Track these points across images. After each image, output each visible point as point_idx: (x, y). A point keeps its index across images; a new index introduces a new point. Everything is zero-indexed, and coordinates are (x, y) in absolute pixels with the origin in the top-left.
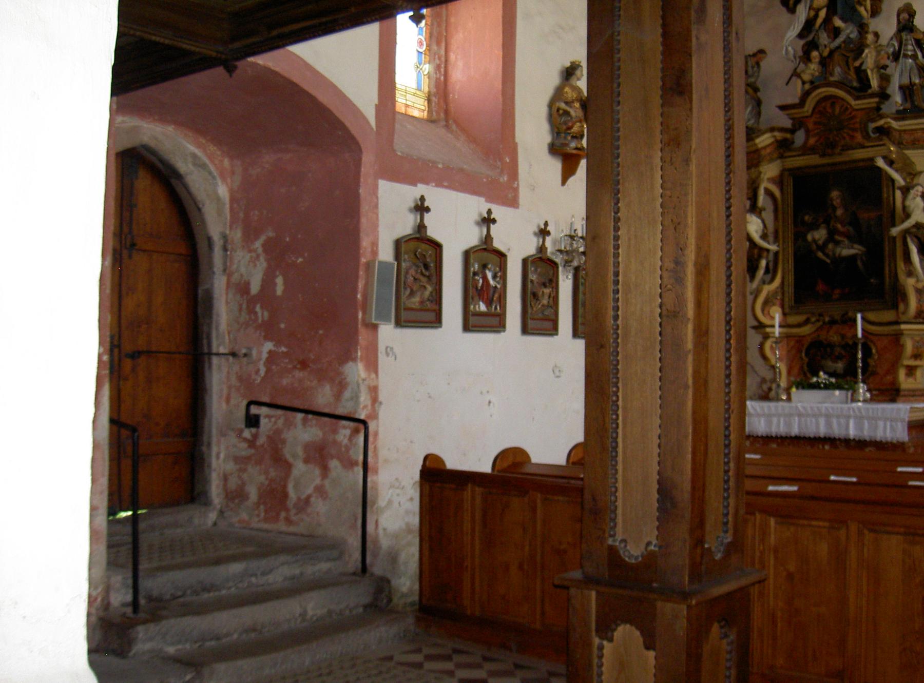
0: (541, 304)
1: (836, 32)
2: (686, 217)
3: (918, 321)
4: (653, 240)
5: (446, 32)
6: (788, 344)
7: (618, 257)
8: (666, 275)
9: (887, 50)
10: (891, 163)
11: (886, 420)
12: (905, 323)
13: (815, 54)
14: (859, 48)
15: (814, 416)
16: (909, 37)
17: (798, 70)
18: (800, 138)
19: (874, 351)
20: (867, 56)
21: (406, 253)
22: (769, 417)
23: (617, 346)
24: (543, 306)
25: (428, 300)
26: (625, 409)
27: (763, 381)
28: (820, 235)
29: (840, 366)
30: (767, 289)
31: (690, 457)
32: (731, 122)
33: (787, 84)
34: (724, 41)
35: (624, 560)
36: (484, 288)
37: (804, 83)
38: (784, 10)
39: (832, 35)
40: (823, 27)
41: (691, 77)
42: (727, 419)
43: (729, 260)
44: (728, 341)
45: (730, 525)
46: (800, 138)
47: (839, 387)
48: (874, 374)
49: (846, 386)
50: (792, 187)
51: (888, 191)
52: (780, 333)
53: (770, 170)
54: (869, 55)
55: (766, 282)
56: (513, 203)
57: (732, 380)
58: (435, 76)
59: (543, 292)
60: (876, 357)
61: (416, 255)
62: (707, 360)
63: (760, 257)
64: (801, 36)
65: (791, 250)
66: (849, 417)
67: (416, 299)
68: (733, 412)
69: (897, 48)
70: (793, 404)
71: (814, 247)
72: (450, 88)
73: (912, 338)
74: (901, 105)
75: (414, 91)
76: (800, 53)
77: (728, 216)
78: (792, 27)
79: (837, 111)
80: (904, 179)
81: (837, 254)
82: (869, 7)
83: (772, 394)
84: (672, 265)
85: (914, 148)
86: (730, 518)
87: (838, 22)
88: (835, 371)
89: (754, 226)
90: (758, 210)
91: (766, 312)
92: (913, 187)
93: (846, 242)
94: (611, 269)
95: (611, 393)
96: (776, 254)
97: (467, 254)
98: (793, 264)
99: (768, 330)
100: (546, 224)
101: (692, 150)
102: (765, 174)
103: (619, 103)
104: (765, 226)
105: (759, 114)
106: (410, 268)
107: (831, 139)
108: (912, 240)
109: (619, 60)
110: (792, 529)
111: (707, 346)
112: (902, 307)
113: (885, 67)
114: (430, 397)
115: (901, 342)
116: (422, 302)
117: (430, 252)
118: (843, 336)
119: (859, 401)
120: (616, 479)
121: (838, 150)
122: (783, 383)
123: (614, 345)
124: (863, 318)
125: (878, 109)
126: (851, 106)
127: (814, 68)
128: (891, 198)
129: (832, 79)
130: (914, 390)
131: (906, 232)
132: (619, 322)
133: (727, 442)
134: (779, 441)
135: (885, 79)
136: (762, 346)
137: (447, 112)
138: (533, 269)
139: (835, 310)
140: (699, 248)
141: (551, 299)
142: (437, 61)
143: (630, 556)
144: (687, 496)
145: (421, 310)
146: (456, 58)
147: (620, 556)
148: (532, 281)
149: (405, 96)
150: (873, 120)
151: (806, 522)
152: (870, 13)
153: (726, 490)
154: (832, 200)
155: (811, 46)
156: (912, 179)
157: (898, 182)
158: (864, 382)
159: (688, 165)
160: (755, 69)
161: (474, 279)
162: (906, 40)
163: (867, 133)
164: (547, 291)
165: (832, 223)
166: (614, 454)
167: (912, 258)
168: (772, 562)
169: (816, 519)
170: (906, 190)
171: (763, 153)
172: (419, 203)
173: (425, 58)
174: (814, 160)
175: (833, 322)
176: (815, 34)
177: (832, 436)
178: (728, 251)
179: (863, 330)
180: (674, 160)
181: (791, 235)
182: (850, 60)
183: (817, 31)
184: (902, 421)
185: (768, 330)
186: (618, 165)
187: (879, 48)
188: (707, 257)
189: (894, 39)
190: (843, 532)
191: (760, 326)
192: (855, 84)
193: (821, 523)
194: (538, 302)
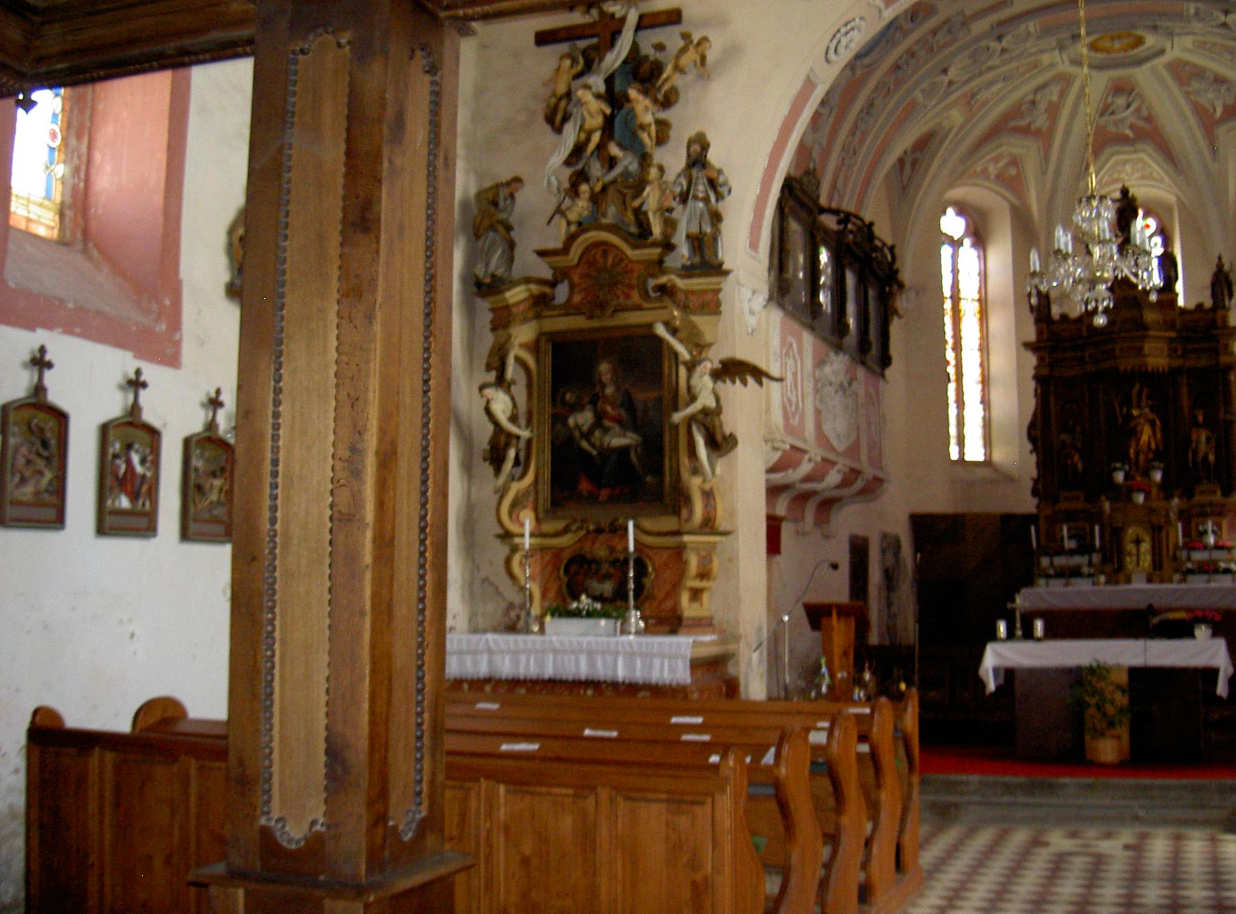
0: (209, 500)
1: (612, 162)
2: (367, 390)
3: (704, 530)
4: (323, 419)
5: (91, 122)
6: (542, 558)
7: (278, 439)
8: (339, 465)
9: (673, 189)
10: (674, 331)
11: (663, 656)
12: (690, 533)
13: (584, 188)
14: (640, 185)
15: (573, 652)
16: (700, 175)
17: (563, 207)
18: (562, 293)
19: (650, 569)
20: (648, 195)
21: (16, 424)
22: (515, 653)
23: (274, 559)
24: (212, 503)
25: (47, 491)
26: (283, 642)
27: (511, 606)
28: (584, 418)
29: (607, 588)
30: (516, 488)
31: (367, 707)
32: (432, 271)
33: (549, 223)
34: (429, 166)
35: (280, 846)
36: (129, 477)
37: (569, 223)
38: (548, 128)
39: (607, 166)
40: (596, 153)
41: (380, 209)
42: (421, 656)
43: (425, 448)
44: (422, 554)
45: (424, 795)
46: (562, 293)
47: (604, 614)
48: (651, 597)
49: (614, 614)
50: (550, 356)
51: (670, 368)
52: (531, 545)
53: (523, 333)
54: (651, 195)
55: (516, 478)
56: (173, 360)
57: (427, 604)
58: (71, 181)
59: (212, 485)
60: (653, 576)
61: (29, 427)
62: (392, 577)
63: (507, 445)
64: (568, 162)
65: (547, 438)
66: (617, 653)
67: (28, 491)
68: (427, 645)
69: (685, 188)
70: (546, 638)
71: (577, 434)
72: (92, 199)
73: (698, 554)
74: (689, 258)
75: (40, 200)
76: (566, 185)
77: (425, 392)
78: (557, 151)
79: (610, 260)
80: (690, 353)
81: (606, 444)
82: (653, 134)
83: (521, 624)
84: (348, 453)
85: (703, 314)
86: (425, 786)
87: (614, 150)
88: (601, 595)
89: (501, 404)
90: (506, 384)
91: (514, 516)
92: (700, 362)
93: (617, 428)
94: (269, 456)
95: (265, 622)
96: (529, 442)
97: (105, 429)
98: (550, 456)
99: (517, 540)
100: (218, 392)
101: (377, 306)
102: (515, 338)
103: (286, 237)
104: (515, 405)
105: (511, 260)
106: (22, 445)
107: (601, 297)
108: (699, 430)
109: (289, 182)
110: (527, 799)
111: (392, 561)
112: (684, 513)
113: (670, 210)
114: (46, 627)
115: (685, 557)
116: (37, 493)
117: (51, 423)
118: (612, 550)
119: (629, 633)
120: (271, 737)
121: (609, 312)
122: (536, 610)
123: (270, 557)
124: (635, 526)
125: (661, 262)
126: (626, 256)
127: (582, 206)
128: (674, 376)
129: (605, 221)
130: (701, 619)
131: (691, 419)
132: (278, 527)
133: (420, 686)
134: (530, 685)
135: (670, 225)
136: (508, 562)
137: (86, 233)
138: (198, 452)
139: (600, 515)
140: (383, 431)
141: (223, 494)
142: (76, 162)
143: (290, 841)
144: (363, 757)
145: (35, 505)
146: (103, 158)
147: (276, 842)
148: (196, 470)
149: (27, 206)
150: (654, 276)
151: (544, 790)
152: (654, 141)
153: (419, 749)
154: (600, 375)
155: (581, 177)
156: (700, 353)
157: (683, 356)
158: (637, 608)
159: (371, 323)
160: (508, 202)
161: (113, 463)
162: (697, 178)
163: (646, 292)
164: (217, 483)
165: (600, 404)
166: (268, 703)
167: (697, 452)
168: (502, 844)
169: (557, 785)
170: (691, 367)
171: (514, 310)
172: (38, 355)
173: (59, 155)
174: (577, 322)
175: (599, 531)
176: (586, 163)
177: (596, 678)
178: (425, 437)
179: (636, 540)
180: (353, 315)
181: (547, 418)
182: (628, 199)
183: (588, 159)
184: (684, 657)
185: (517, 540)
186: (282, 318)
187: (664, 186)
188: (393, 444)
189: (682, 175)
190: (591, 801)
191: (506, 536)
192: (633, 229)
193: (564, 791)
194: (205, 498)
